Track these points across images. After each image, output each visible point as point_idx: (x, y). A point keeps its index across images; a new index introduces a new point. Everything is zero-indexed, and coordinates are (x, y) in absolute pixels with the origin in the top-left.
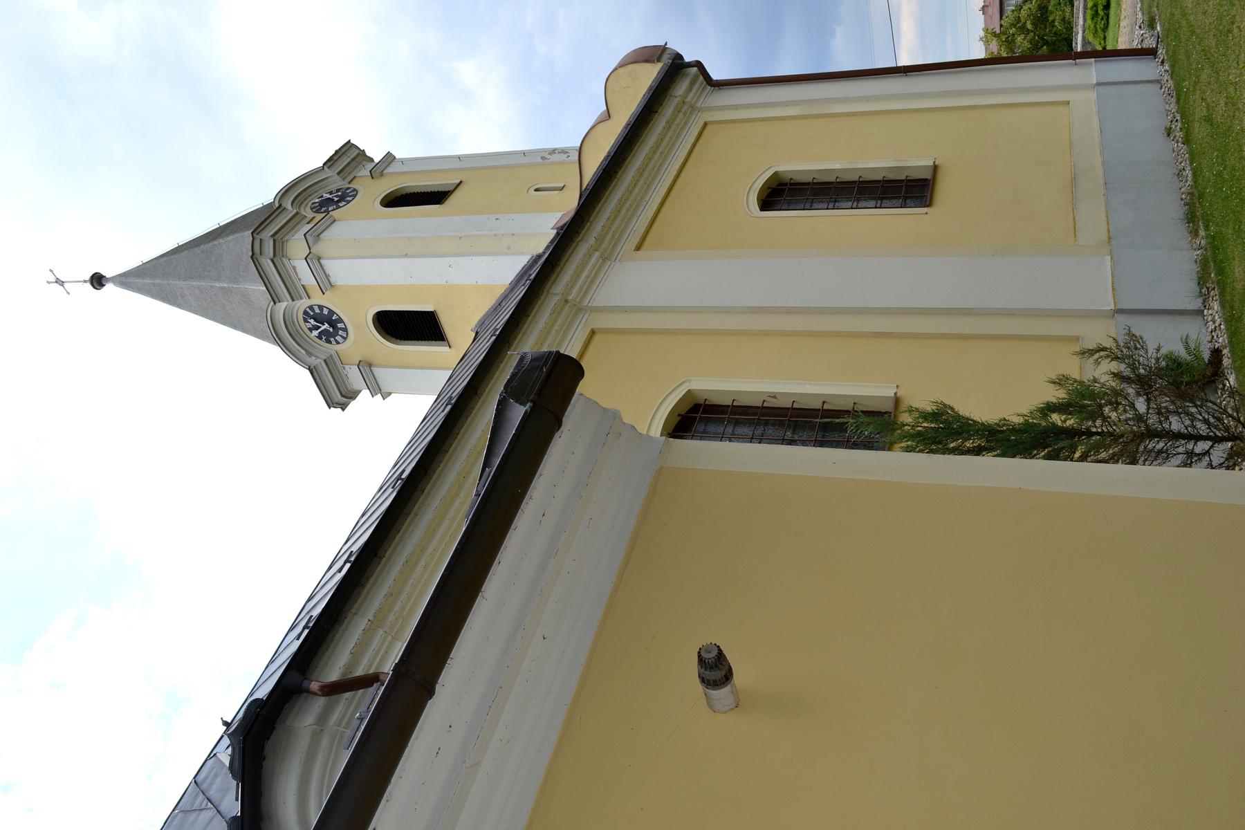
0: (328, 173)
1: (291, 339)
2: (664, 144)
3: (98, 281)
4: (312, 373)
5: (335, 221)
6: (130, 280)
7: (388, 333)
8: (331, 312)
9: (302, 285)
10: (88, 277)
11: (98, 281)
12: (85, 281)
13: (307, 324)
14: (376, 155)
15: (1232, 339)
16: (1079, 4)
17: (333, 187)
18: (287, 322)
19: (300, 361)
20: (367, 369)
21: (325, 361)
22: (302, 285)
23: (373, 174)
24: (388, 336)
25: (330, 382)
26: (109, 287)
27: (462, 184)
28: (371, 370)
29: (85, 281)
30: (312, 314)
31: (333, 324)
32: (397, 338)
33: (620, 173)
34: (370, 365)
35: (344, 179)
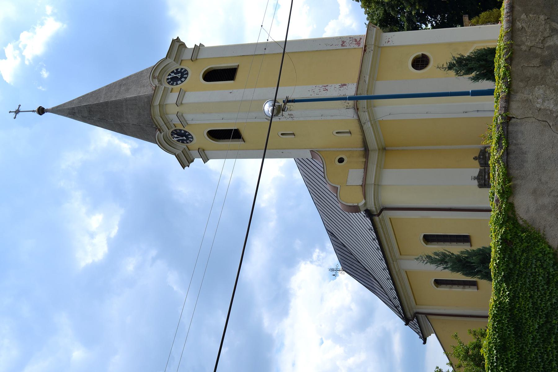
0: (169, 61)
1: (165, 142)
2: (385, 231)
3: (41, 111)
4: (447, 356)
5: (185, 92)
6: (57, 110)
7: (213, 137)
8: (186, 132)
9: (173, 124)
10: (36, 109)
11: (41, 111)
12: (34, 111)
13: (172, 136)
14: (190, 45)
15: (475, 255)
16: (505, 4)
17: (174, 69)
18: (165, 138)
19: (161, 145)
20: (202, 152)
21: (182, 152)
22: (173, 124)
23: (193, 60)
24: (213, 138)
25: (185, 161)
26: (46, 114)
27: (239, 66)
28: (204, 153)
29: (34, 111)
30: (176, 132)
31: (186, 136)
32: (217, 139)
33: (383, 247)
34: (204, 150)
35: (172, 59)
